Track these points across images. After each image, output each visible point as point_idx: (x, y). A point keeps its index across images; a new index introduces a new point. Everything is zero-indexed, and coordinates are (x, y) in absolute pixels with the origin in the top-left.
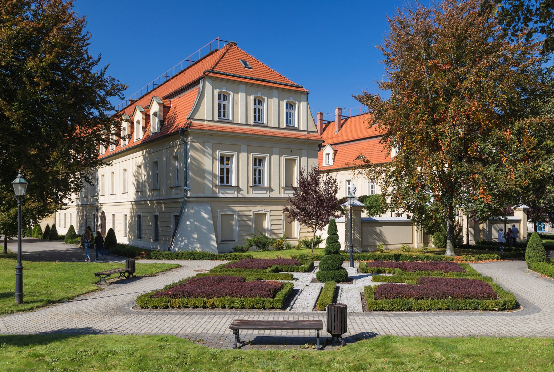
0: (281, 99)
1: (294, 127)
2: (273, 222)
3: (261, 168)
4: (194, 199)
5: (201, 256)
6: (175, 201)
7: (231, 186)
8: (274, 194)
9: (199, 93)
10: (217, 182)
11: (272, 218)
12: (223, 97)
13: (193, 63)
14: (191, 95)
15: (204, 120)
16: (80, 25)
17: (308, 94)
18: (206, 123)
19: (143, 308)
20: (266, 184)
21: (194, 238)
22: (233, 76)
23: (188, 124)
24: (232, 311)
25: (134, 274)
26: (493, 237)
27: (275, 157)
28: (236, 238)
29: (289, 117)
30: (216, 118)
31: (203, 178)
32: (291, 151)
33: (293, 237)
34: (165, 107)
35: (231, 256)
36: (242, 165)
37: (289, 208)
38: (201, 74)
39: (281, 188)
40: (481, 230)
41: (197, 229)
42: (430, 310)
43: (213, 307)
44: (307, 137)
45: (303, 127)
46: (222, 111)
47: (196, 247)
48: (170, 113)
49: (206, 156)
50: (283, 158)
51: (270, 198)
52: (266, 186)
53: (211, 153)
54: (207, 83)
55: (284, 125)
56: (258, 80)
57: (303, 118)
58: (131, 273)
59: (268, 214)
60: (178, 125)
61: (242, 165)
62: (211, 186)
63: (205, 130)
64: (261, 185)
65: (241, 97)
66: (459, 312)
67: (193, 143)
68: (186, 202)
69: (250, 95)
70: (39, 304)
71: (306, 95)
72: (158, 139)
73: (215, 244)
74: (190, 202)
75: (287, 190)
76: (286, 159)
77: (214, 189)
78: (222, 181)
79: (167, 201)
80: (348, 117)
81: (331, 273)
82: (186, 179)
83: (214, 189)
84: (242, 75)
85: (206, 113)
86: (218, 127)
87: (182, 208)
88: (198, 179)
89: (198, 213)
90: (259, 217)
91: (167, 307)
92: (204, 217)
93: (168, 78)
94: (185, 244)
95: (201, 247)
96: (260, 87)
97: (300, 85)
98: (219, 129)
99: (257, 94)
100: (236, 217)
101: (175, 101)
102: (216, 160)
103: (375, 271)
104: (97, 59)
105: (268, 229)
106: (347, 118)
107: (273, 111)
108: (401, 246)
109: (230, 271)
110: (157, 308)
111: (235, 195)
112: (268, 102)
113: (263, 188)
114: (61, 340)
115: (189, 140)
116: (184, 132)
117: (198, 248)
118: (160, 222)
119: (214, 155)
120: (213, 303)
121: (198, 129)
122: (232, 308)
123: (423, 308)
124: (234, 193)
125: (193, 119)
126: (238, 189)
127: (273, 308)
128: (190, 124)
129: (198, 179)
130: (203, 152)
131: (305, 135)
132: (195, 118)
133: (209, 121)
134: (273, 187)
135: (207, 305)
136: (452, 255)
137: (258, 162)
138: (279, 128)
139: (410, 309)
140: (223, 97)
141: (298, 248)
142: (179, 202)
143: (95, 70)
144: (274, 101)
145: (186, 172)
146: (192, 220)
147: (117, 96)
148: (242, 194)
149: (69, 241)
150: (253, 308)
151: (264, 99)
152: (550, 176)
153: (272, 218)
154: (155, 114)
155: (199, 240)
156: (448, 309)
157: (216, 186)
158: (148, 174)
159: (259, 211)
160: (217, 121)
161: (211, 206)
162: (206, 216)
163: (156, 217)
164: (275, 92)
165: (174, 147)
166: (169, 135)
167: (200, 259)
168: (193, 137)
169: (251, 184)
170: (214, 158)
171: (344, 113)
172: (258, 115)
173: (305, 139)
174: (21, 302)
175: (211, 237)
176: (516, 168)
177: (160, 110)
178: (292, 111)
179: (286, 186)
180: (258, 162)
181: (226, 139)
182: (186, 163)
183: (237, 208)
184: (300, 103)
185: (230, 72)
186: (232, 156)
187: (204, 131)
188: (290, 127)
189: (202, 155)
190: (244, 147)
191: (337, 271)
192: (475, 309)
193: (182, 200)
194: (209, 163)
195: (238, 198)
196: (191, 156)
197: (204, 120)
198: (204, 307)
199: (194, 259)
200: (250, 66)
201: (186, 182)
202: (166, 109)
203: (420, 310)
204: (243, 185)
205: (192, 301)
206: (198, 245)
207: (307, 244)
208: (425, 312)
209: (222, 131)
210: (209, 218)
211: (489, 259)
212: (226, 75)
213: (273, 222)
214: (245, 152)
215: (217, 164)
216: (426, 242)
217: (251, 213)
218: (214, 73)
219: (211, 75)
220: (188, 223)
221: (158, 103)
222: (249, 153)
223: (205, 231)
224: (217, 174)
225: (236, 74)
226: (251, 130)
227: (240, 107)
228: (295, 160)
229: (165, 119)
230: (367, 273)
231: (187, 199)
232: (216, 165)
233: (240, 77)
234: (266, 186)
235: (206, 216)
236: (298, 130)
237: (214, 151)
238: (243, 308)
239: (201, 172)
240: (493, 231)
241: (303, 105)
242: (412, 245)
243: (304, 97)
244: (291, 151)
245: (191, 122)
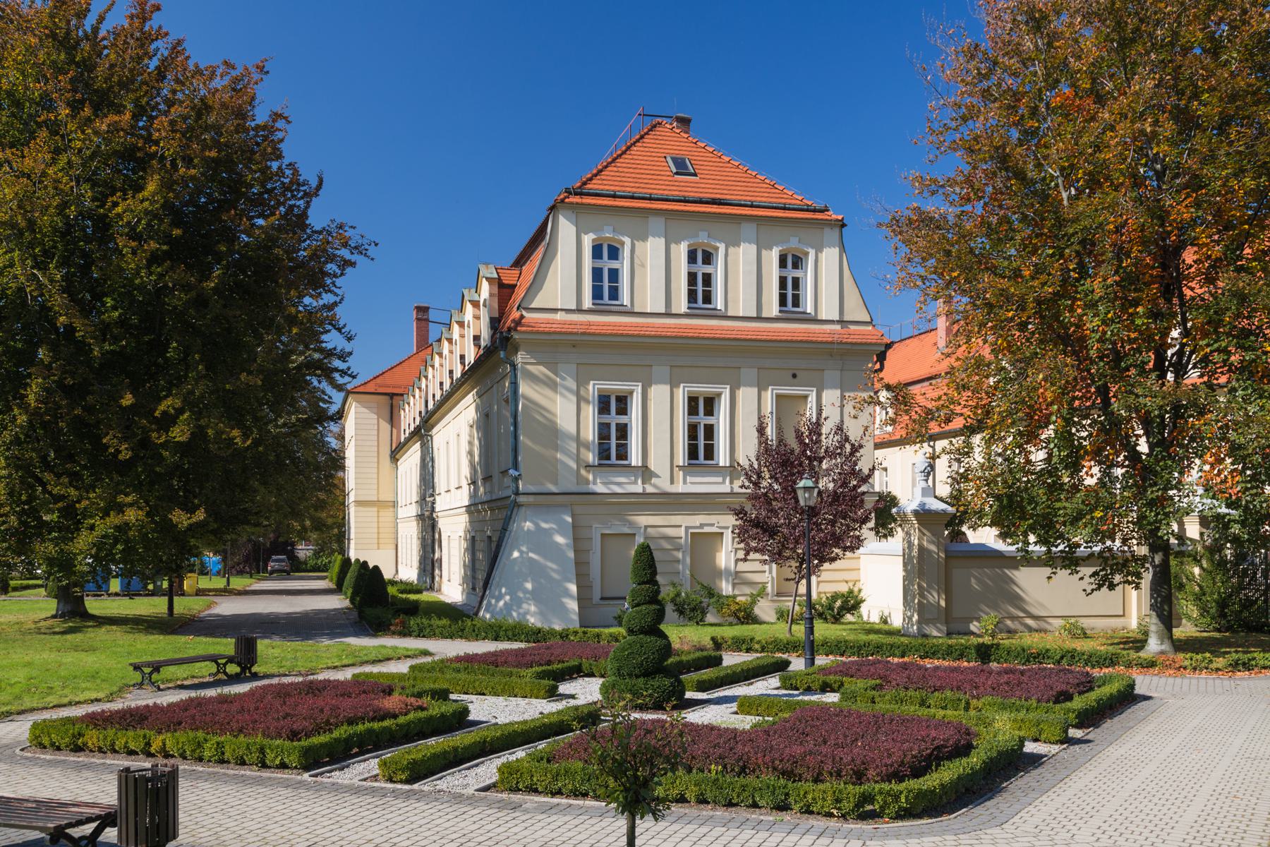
0: (761, 246)
1: (805, 313)
4: (531, 499)
7: (629, 466)
10: (591, 457)
15: (555, 310)
17: (843, 225)
18: (559, 316)
21: (525, 591)
25: (254, 669)
30: (587, 303)
32: (794, 376)
39: (676, 469)
45: (829, 310)
47: (527, 612)
49: (562, 395)
52: (721, 464)
53: (575, 388)
56: (700, 202)
61: (658, 417)
62: (575, 466)
63: (555, 333)
65: (744, 254)
67: (528, 367)
69: (678, 242)
71: (837, 230)
73: (573, 605)
76: (778, 396)
78: (604, 453)
83: (583, 472)
84: (657, 193)
92: (557, 544)
94: (506, 603)
95: (541, 613)
96: (704, 218)
98: (593, 329)
99: (788, 241)
102: (588, 402)
104: (314, 183)
105: (727, 570)
111: (638, 488)
112: (726, 255)
113: (717, 470)
115: (520, 358)
119: (582, 392)
121: (537, 332)
124: (724, 482)
125: (527, 309)
126: (645, 472)
130: (553, 386)
131: (832, 333)
132: (532, 306)
134: (652, 466)
136: (1162, 652)
138: (759, 318)
146: (524, 549)
148: (655, 486)
151: (807, 254)
155: (536, 596)
157: (588, 466)
159: (702, 526)
160: (686, 315)
161: (573, 516)
162: (560, 539)
164: (749, 229)
168: (528, 352)
169: (681, 458)
170: (581, 400)
172: (790, 293)
173: (832, 343)
183: (643, 520)
184: (819, 250)
187: (553, 337)
190: (661, 370)
195: (644, 494)
197: (555, 310)
204: (658, 462)
206: (533, 608)
209: (599, 334)
214: (665, 383)
215: (590, 412)
217: (682, 533)
220: (516, 554)
222: (674, 385)
223: (556, 576)
224: (591, 438)
226: (680, 327)
228: (806, 397)
230: (797, 689)
232: (587, 417)
233: (650, 199)
234: (721, 464)
237: (581, 382)
239: (551, 433)
241: (830, 258)
242: (1122, 620)
244: (794, 376)
245: (522, 317)
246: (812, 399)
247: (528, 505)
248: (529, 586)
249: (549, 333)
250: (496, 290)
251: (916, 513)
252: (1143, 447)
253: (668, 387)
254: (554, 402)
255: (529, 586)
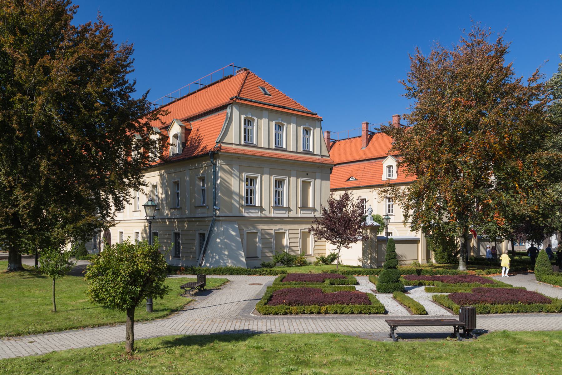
0: (270, 120)
2: (292, 240)
3: (252, 188)
4: (224, 218)
5: (238, 272)
6: (202, 219)
7: (255, 206)
8: (292, 214)
9: (227, 118)
10: (244, 203)
11: (291, 236)
12: (249, 122)
13: (202, 87)
14: (218, 119)
15: (232, 144)
16: (129, 51)
18: (233, 146)
19: (265, 314)
20: (285, 205)
22: (257, 102)
23: (219, 147)
24: (342, 316)
26: (481, 254)
27: (293, 179)
28: (259, 255)
29: (278, 138)
30: (243, 142)
31: (232, 198)
33: (308, 254)
34: (186, 129)
35: (266, 271)
36: (264, 186)
37: (315, 227)
38: (227, 100)
40: (471, 248)
41: (227, 247)
42: (504, 313)
43: (326, 313)
44: (321, 161)
45: (317, 152)
46: (248, 134)
48: (192, 135)
50: (300, 180)
51: (288, 218)
54: (234, 109)
55: (273, 146)
56: (283, 107)
57: (316, 142)
58: (202, 286)
59: (287, 233)
60: (205, 147)
61: (264, 186)
62: (238, 206)
64: (253, 204)
66: (528, 314)
67: (223, 166)
68: (215, 220)
70: (165, 313)
72: (179, 161)
74: (219, 221)
75: (276, 210)
77: (241, 208)
79: (190, 219)
80: (336, 141)
81: (392, 285)
82: (215, 198)
83: (241, 208)
85: (234, 137)
86: (244, 150)
87: (212, 227)
88: (226, 198)
89: (227, 230)
90: (280, 235)
91: (287, 314)
93: (174, 100)
96: (281, 113)
97: (314, 112)
98: (246, 153)
99: (278, 120)
100: (259, 234)
101: (194, 125)
102: (243, 181)
103: (417, 284)
105: (287, 246)
106: (335, 141)
107: (292, 137)
108: (412, 262)
109: (293, 284)
110: (277, 314)
111: (259, 214)
113: (282, 208)
114: (229, 341)
115: (219, 162)
116: (214, 155)
117: (230, 264)
118: (182, 239)
119: (241, 177)
120: (327, 310)
122: (343, 313)
123: (499, 311)
126: (261, 209)
127: (377, 313)
128: (220, 147)
129: (226, 198)
130: (231, 174)
132: (224, 141)
133: (236, 145)
135: (321, 311)
137: (279, 183)
139: (489, 313)
140: (249, 122)
141: (317, 264)
142: (206, 221)
143: (135, 96)
144: (292, 127)
145: (215, 193)
147: (158, 120)
148: (264, 214)
149: (80, 257)
150: (360, 313)
152: (558, 202)
153: (291, 236)
154: (176, 136)
155: (229, 256)
156: (518, 312)
158: (166, 193)
160: (243, 145)
161: (238, 225)
162: (233, 233)
163: (177, 235)
165: (199, 168)
166: (196, 157)
167: (238, 274)
168: (223, 160)
170: (240, 180)
171: (333, 137)
173: (320, 163)
174: (152, 311)
175: (240, 254)
176: (528, 195)
177: (182, 133)
178: (250, 128)
179: (302, 207)
180: (279, 183)
181: (252, 163)
182: (215, 184)
183: (261, 227)
184: (314, 129)
185: (254, 99)
186: (256, 178)
188: (279, 148)
189: (229, 176)
191: (396, 284)
192: (540, 312)
193: (212, 219)
194: (236, 185)
195: (261, 217)
196: (221, 177)
197: (232, 144)
198: (319, 313)
199: (231, 274)
200: (268, 93)
201: (215, 202)
202: (187, 131)
203: (496, 313)
204: (265, 206)
205: (308, 308)
207: (325, 261)
208: (501, 315)
210: (236, 236)
211: (496, 273)
212: (251, 101)
213: (292, 240)
215: (243, 184)
216: (428, 258)
218: (241, 99)
219: (237, 101)
221: (180, 126)
222: (271, 175)
223: (234, 248)
225: (259, 101)
226: (277, 154)
227: (263, 132)
228: (310, 182)
229: (186, 140)
231: (217, 219)
233: (263, 104)
234: (257, 205)
235: (233, 233)
236: (312, 154)
237: (241, 173)
238: (352, 313)
239: (229, 192)
240: (481, 248)
241: (318, 130)
243: (318, 123)
246: (312, 184)
247: (223, 221)
248: (226, 253)
249: (231, 153)
250: (184, 131)
251: (370, 226)
252: (480, 208)
253: (295, 178)
254: (231, 181)
255: (226, 253)
